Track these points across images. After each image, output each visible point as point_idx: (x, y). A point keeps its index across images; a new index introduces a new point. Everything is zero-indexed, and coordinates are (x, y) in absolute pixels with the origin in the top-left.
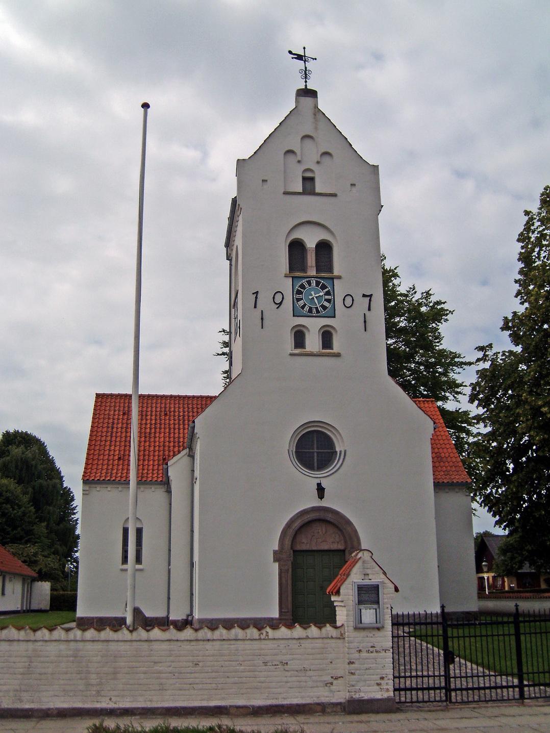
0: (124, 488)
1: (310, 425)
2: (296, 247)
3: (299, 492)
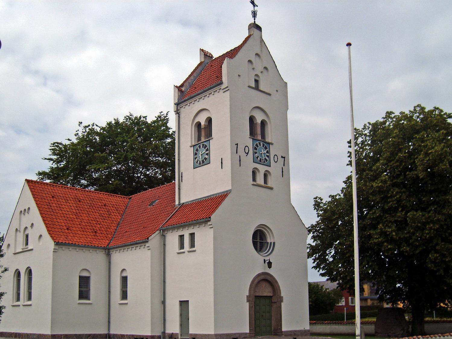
0: (66, 248)
1: (264, 227)
2: (252, 119)
3: (255, 264)
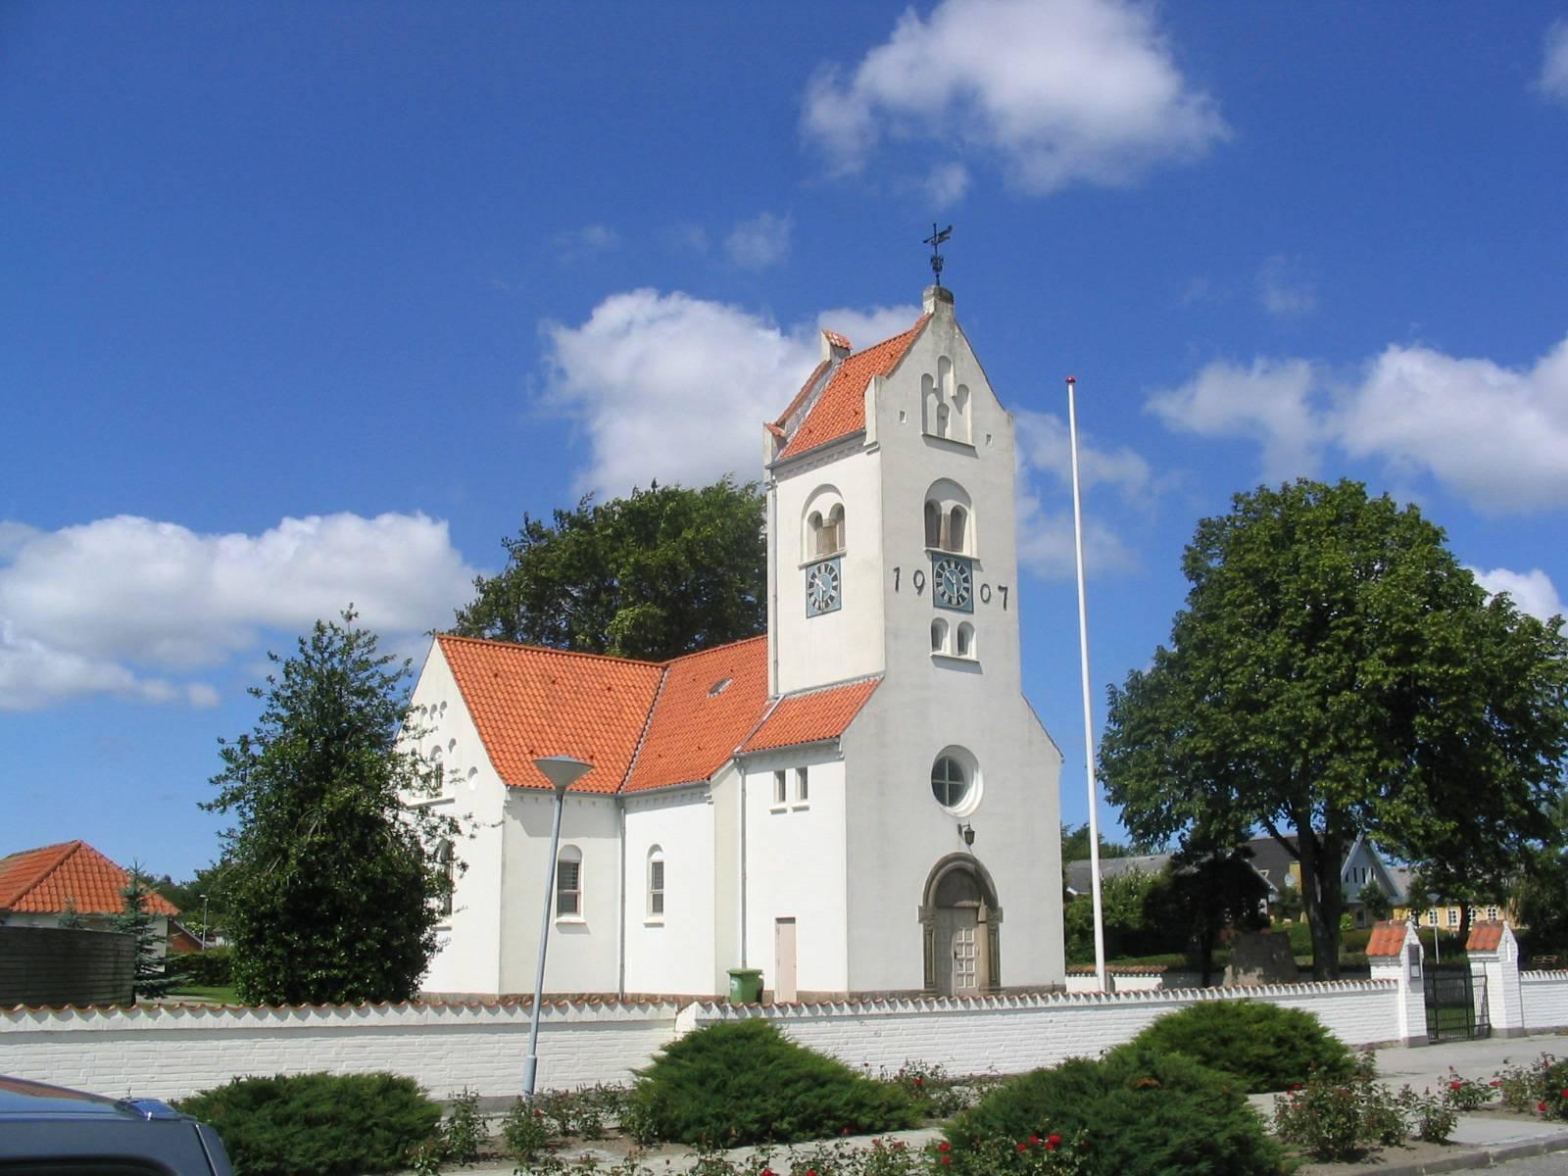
2: (931, 508)
